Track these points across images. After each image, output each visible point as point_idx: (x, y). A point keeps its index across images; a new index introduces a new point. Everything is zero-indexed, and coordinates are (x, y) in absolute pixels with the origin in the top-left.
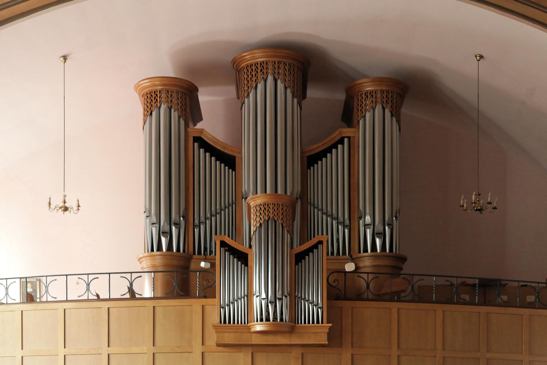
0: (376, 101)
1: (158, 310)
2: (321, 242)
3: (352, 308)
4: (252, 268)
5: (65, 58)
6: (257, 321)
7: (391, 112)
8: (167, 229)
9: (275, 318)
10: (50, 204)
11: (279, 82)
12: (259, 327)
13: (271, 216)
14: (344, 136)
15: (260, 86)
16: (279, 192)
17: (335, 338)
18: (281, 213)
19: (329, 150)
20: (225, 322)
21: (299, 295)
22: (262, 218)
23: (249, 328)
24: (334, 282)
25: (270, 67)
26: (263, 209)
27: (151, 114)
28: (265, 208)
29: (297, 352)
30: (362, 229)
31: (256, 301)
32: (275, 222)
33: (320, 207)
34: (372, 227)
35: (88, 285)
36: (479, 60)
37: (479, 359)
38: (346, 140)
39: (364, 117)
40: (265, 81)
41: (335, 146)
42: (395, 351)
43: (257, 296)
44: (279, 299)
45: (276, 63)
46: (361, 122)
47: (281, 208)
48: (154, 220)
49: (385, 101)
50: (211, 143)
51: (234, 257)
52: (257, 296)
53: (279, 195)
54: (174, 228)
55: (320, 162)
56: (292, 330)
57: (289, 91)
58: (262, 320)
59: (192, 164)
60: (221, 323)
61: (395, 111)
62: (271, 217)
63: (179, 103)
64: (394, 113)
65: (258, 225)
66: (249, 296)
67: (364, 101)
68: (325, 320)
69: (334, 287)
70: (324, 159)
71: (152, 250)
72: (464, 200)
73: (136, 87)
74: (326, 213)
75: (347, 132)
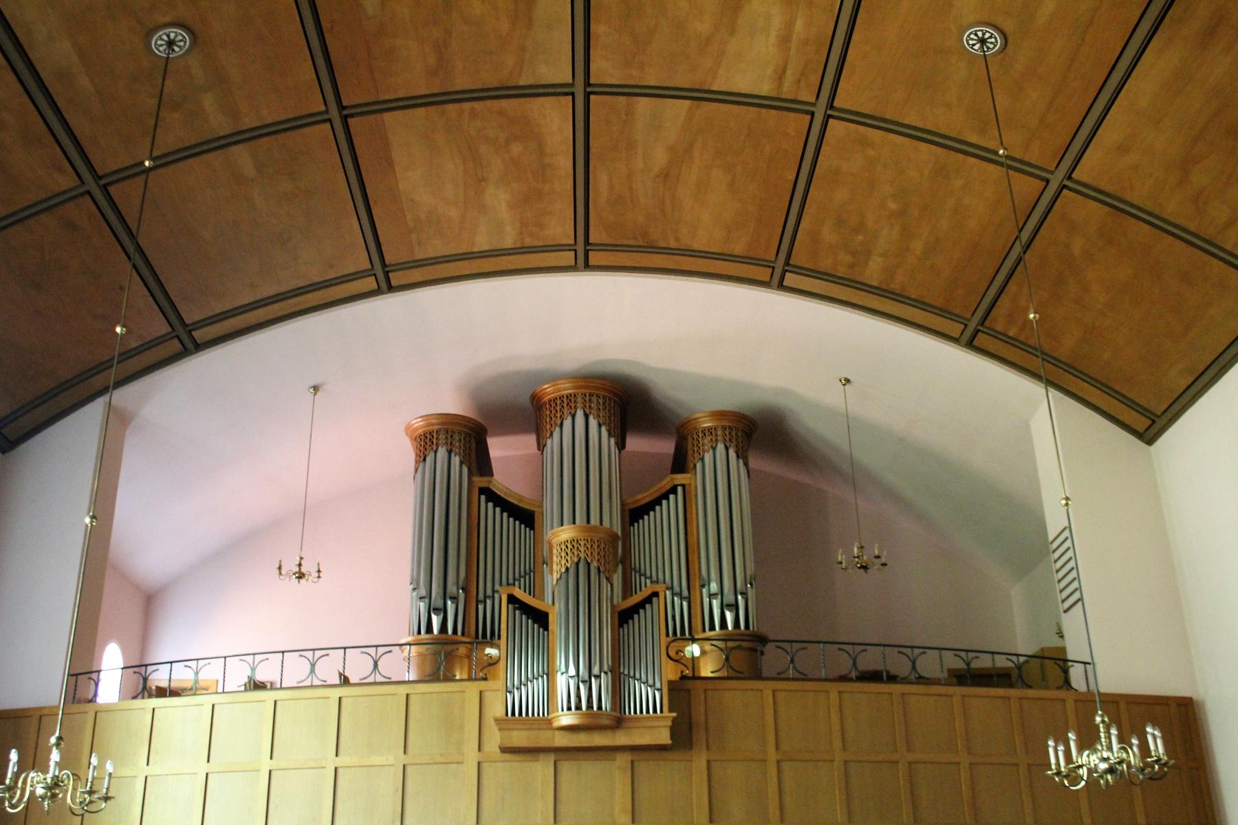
1: (413, 699)
2: (656, 594)
4: (554, 655)
7: (737, 453)
8: (440, 604)
9: (590, 706)
10: (280, 568)
11: (591, 418)
12: (567, 719)
15: (567, 423)
16: (593, 522)
17: (684, 735)
19: (657, 502)
23: (549, 722)
25: (579, 399)
29: (623, 760)
30: (706, 600)
32: (588, 564)
33: (648, 574)
35: (313, 665)
37: (897, 762)
38: (680, 489)
39: (702, 459)
40: (573, 417)
46: (699, 466)
48: (423, 592)
54: (449, 602)
55: (646, 517)
57: (604, 429)
58: (569, 709)
66: (549, 674)
70: (652, 513)
71: (419, 633)
73: (409, 430)
75: (680, 478)
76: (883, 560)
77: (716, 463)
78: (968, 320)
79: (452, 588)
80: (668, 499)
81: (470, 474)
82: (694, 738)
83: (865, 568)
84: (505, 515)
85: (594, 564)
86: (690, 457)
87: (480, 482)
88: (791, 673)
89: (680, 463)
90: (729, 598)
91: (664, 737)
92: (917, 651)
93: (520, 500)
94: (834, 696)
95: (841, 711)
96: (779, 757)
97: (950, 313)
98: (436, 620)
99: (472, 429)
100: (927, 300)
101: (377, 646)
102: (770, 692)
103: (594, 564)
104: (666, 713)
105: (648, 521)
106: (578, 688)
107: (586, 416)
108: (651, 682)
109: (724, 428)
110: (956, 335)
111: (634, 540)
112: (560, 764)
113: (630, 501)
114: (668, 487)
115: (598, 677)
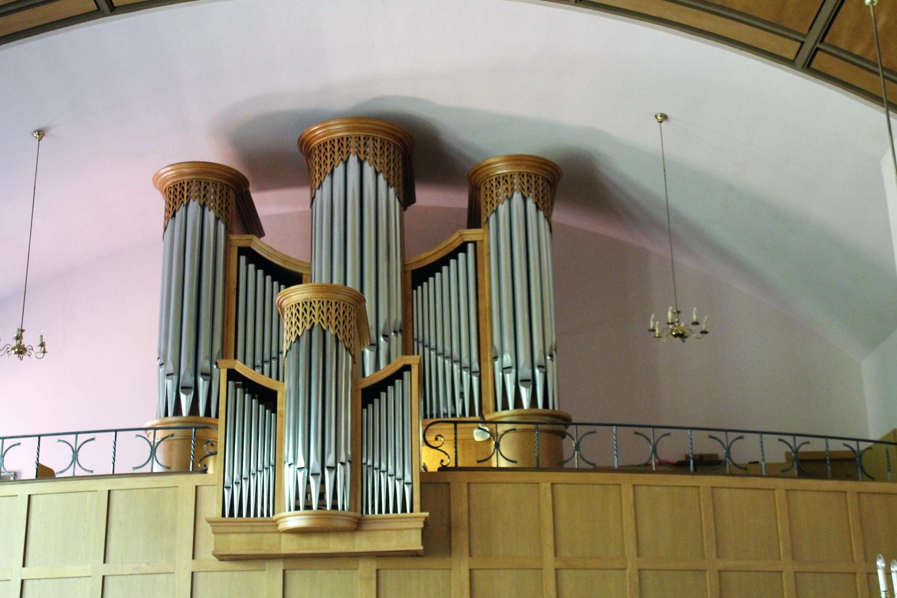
0: (512, 189)
2: (407, 368)
3: (469, 484)
6: (290, 510)
12: (295, 520)
13: (316, 321)
14: (466, 240)
15: (339, 171)
17: (439, 539)
18: (334, 316)
19: (444, 261)
20: (231, 514)
21: (370, 463)
22: (300, 326)
23: (275, 523)
24: (436, 439)
25: (353, 143)
26: (301, 310)
27: (174, 215)
28: (305, 310)
29: (367, 568)
30: (499, 375)
32: (324, 332)
33: (433, 345)
34: (514, 370)
35: (75, 453)
36: (661, 122)
38: (470, 247)
39: (496, 211)
40: (346, 163)
41: (454, 255)
42: (549, 563)
43: (290, 465)
44: (329, 468)
45: (362, 138)
46: (492, 219)
47: (334, 307)
48: (170, 368)
49: (525, 188)
50: (265, 256)
51: (253, 397)
52: (290, 465)
53: (335, 286)
55: (431, 279)
56: (358, 525)
57: (381, 177)
59: (235, 286)
60: (223, 515)
61: (541, 202)
62: (316, 324)
63: (217, 198)
64: (540, 206)
65: (293, 339)
66: (275, 467)
67: (494, 189)
68: (417, 506)
70: (438, 275)
71: (166, 415)
72: (655, 323)
75: (472, 234)
76: (704, 327)
78: (805, 36)
79: (204, 364)
80: (456, 258)
82: (453, 544)
83: (682, 336)
84: (269, 278)
85: (331, 332)
86: (483, 211)
87: (240, 240)
88: (575, 463)
89: (475, 219)
90: (525, 372)
91: (414, 542)
92: (732, 436)
93: (285, 262)
94: (627, 491)
95: (635, 507)
96: (557, 565)
97: (783, 28)
99: (230, 180)
100: (754, 13)
101: (77, 433)
102: (549, 485)
103: (331, 332)
104: (417, 512)
105: (434, 283)
106: (308, 482)
107: (361, 163)
108: (399, 474)
109: (521, 175)
110: (791, 56)
113: (413, 260)
114: (457, 244)
115: (333, 468)
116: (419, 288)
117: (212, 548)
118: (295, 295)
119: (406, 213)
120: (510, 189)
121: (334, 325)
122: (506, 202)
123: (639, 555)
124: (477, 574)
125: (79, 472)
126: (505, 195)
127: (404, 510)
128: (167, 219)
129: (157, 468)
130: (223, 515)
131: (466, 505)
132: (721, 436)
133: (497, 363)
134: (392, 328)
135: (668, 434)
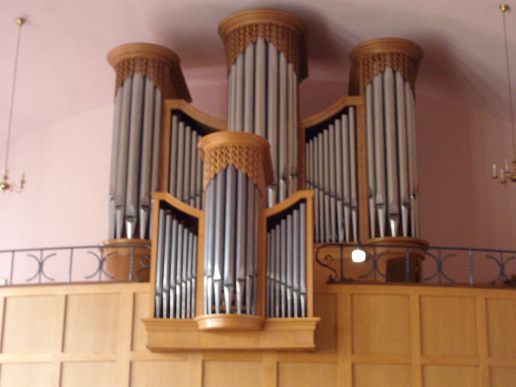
1: (72, 301)
2: (303, 201)
3: (352, 295)
5: (23, 21)
6: (208, 313)
12: (210, 321)
13: (230, 162)
14: (348, 104)
15: (249, 50)
17: (327, 339)
19: (331, 121)
23: (196, 324)
24: (326, 258)
25: (261, 29)
27: (122, 84)
28: (222, 153)
31: (207, 282)
34: (384, 206)
35: (41, 264)
36: (504, 12)
38: (351, 111)
39: (372, 83)
40: (255, 44)
41: (338, 116)
42: (417, 359)
45: (267, 25)
47: (245, 151)
55: (320, 135)
57: (282, 55)
64: (406, 78)
66: (196, 276)
68: (310, 312)
69: (326, 266)
70: (325, 132)
71: (115, 237)
74: (329, 194)
75: (351, 101)
77: (384, 86)
81: (163, 98)
82: (339, 343)
87: (172, 104)
89: (354, 89)
90: (393, 208)
92: (506, 256)
98: (130, 227)
101: (42, 250)
106: (222, 292)
109: (392, 54)
111: (309, 156)
112: (208, 365)
116: (311, 142)
117: (145, 342)
118: (213, 141)
119: (301, 85)
120: (383, 64)
121: (244, 165)
122: (380, 75)
123: (489, 355)
124: (357, 367)
125: (44, 280)
126: (379, 69)
127: (300, 315)
128: (117, 87)
129: (104, 278)
130: (155, 316)
131: (349, 312)
132: (497, 255)
133: (371, 201)
134: (290, 172)
135: (453, 255)
